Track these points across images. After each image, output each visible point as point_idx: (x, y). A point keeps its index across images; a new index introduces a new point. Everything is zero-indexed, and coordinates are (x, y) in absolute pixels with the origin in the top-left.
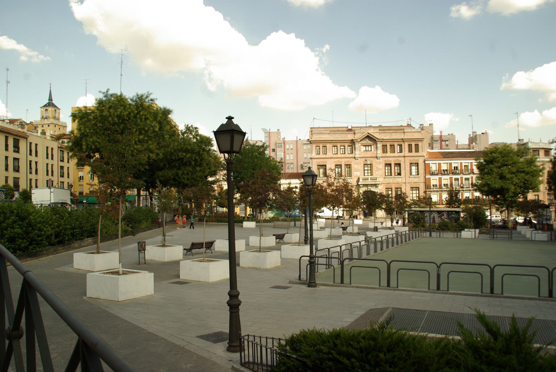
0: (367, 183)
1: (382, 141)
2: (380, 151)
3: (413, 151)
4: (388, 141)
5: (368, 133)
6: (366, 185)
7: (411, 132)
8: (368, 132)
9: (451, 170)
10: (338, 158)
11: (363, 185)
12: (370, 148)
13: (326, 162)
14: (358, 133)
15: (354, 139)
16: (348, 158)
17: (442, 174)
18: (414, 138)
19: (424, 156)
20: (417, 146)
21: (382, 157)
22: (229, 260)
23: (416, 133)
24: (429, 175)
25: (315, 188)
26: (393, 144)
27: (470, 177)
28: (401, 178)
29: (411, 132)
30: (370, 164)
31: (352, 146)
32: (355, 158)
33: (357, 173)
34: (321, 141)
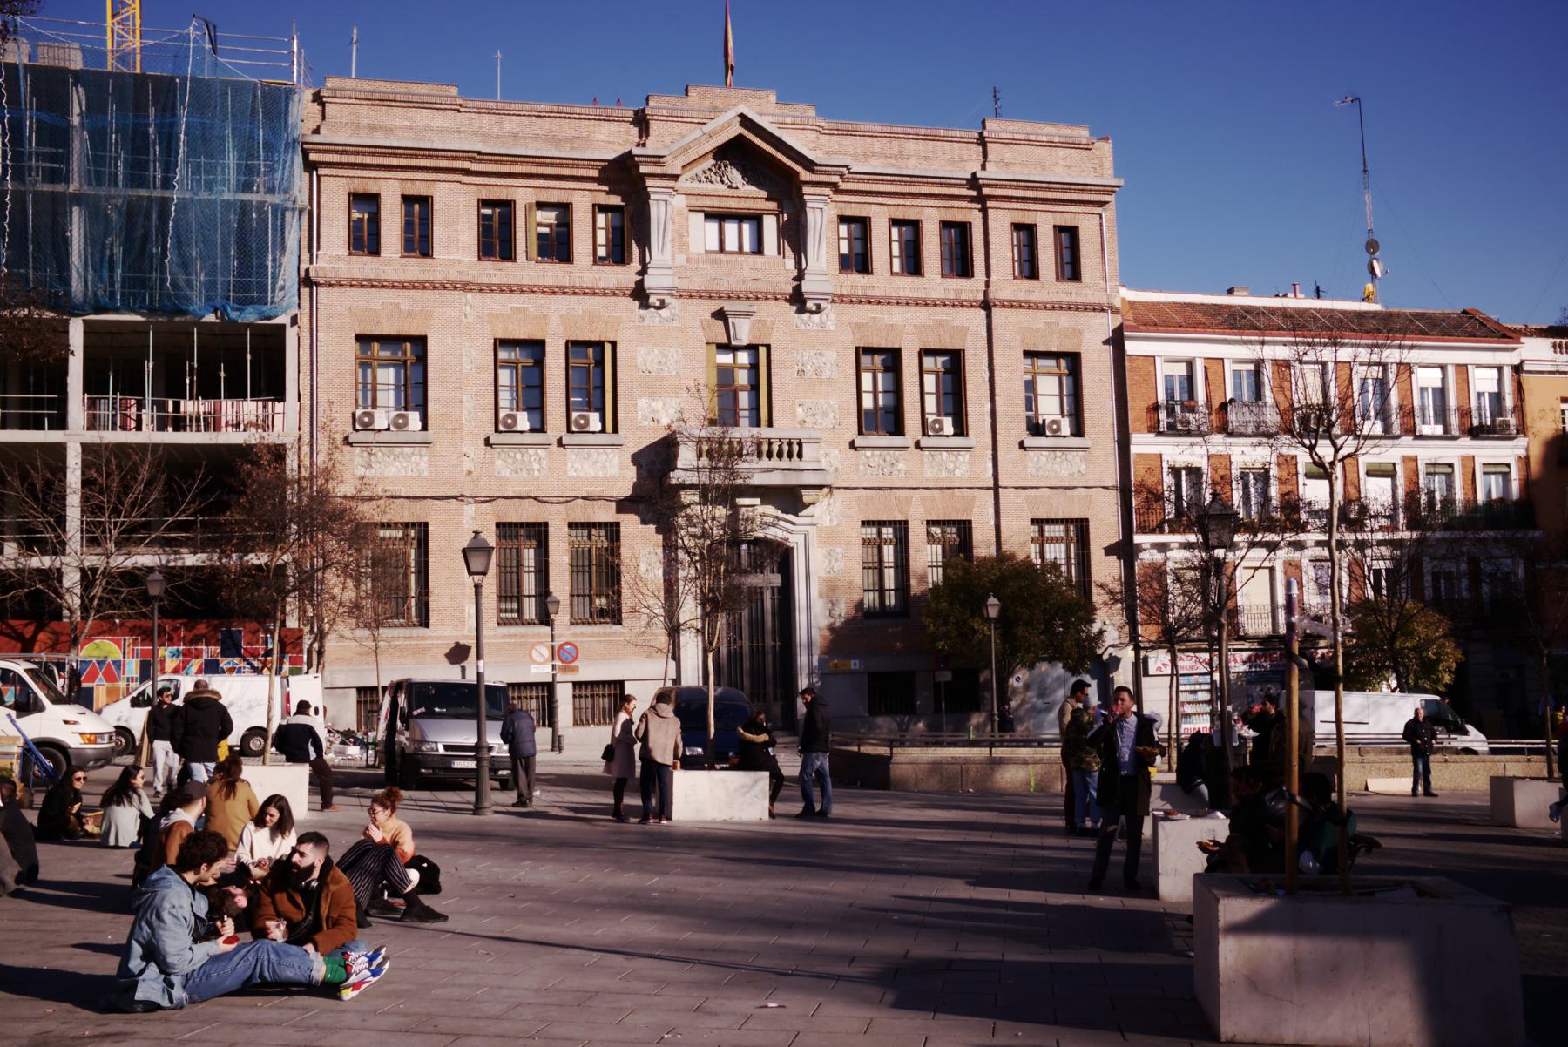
3: (1042, 272)
4: (462, 164)
5: (745, 121)
10: (521, 289)
13: (1078, 333)
15: (636, 151)
16: (593, 292)
18: (380, 140)
20: (1069, 236)
21: (841, 299)
23: (1061, 152)
25: (1180, 527)
29: (1029, 143)
30: (752, 348)
31: (756, 219)
32: (640, 294)
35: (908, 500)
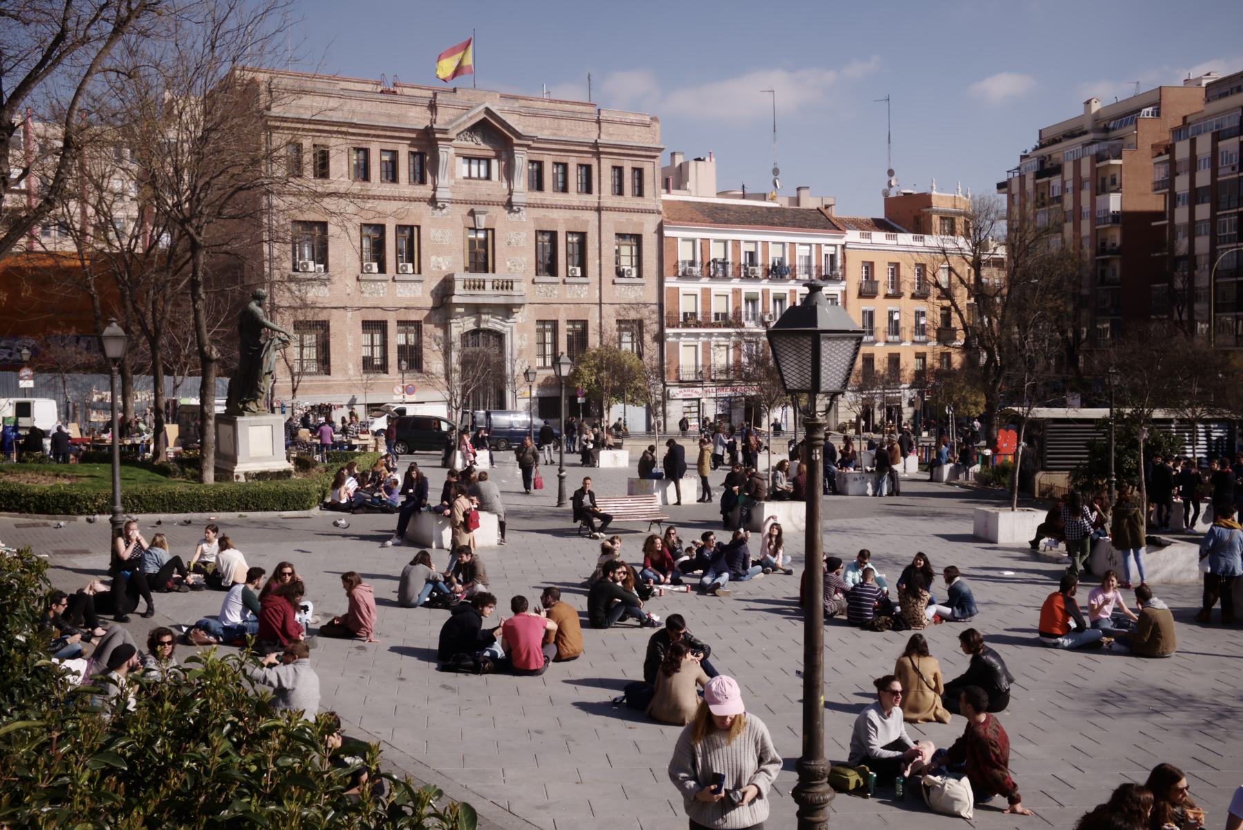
0: (480, 301)
1: (529, 147)
2: (521, 182)
4: (570, 146)
5: (488, 111)
6: (475, 310)
7: (622, 123)
8: (487, 105)
9: (737, 264)
11: (466, 306)
12: (483, 168)
14: (447, 106)
17: (713, 277)
19: (659, 213)
21: (529, 205)
22: (972, 533)
23: (636, 128)
24: (675, 279)
26: (364, 146)
27: (787, 292)
28: (587, 284)
29: (622, 123)
30: (486, 230)
32: (433, 201)
33: (440, 259)
34: (632, 148)
35: (559, 309)
